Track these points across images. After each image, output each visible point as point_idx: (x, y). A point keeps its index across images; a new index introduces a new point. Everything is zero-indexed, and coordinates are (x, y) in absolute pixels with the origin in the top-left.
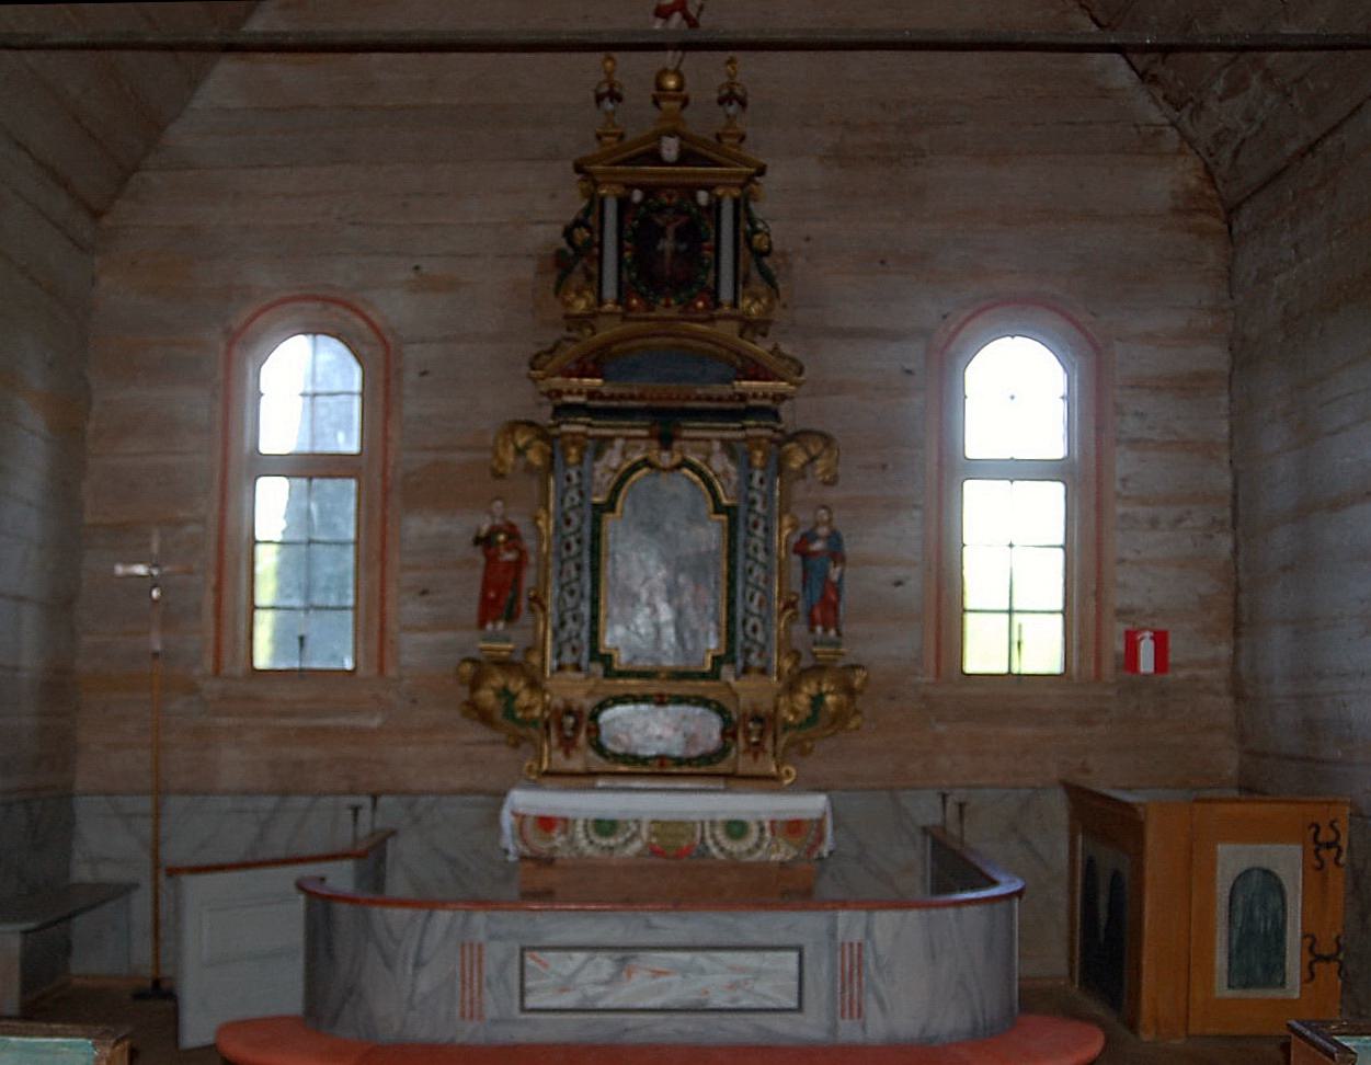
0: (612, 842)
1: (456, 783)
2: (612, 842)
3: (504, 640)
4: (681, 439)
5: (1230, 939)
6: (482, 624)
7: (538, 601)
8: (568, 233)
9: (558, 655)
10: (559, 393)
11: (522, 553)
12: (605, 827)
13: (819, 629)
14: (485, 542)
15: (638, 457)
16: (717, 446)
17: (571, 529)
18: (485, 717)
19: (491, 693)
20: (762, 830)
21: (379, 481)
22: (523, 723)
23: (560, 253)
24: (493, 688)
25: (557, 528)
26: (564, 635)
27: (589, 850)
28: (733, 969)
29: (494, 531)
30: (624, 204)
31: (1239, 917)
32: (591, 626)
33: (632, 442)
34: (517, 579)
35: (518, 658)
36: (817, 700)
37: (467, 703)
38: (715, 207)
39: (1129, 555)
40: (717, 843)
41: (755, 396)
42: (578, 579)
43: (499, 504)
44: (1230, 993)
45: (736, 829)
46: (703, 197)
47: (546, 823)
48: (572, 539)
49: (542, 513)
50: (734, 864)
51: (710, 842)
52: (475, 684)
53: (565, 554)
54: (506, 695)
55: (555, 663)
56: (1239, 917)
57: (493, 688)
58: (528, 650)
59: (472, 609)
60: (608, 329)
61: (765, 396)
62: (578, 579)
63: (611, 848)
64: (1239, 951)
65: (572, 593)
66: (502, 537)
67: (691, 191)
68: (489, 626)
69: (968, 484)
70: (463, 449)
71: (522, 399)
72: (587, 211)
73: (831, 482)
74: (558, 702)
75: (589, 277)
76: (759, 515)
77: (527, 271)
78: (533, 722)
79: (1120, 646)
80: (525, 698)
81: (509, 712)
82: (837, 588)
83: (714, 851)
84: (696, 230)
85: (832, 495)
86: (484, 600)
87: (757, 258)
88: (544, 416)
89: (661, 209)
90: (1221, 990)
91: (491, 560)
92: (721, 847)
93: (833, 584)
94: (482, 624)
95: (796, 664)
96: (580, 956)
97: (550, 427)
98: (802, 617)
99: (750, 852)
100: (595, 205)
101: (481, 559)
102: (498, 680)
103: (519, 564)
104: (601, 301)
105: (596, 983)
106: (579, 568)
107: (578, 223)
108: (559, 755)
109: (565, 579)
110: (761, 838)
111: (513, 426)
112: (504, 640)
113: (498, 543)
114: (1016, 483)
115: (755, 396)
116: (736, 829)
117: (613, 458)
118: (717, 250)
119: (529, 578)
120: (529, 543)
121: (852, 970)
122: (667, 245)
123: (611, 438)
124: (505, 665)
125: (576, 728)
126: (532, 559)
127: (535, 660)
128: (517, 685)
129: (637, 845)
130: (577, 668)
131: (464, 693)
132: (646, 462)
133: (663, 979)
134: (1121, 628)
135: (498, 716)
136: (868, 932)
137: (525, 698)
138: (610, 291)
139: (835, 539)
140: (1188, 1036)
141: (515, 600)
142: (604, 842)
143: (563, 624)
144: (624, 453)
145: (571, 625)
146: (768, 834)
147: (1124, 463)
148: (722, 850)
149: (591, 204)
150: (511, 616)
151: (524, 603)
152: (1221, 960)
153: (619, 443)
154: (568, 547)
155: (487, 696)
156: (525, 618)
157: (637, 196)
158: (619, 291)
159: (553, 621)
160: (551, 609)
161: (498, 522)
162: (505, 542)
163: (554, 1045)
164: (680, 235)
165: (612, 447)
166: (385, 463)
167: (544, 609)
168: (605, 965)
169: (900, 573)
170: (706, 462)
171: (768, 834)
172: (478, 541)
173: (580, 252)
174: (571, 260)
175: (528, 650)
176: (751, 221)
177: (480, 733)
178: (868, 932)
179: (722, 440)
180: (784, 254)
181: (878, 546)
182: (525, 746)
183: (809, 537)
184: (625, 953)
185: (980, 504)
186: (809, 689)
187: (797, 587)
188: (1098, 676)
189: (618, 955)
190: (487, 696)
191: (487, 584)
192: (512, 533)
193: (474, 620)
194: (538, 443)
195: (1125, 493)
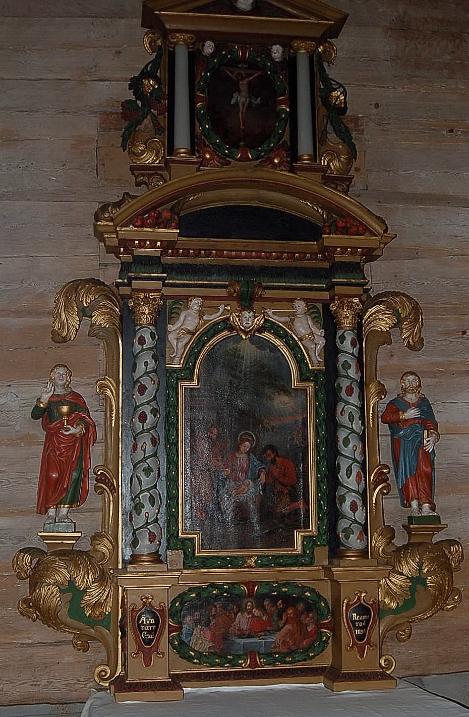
3: (65, 527)
4: (261, 299)
6: (43, 509)
7: (107, 482)
8: (135, 84)
9: (135, 543)
11: (90, 427)
13: (414, 504)
14: (44, 414)
15: (215, 317)
16: (300, 306)
17: (144, 399)
18: (49, 617)
19: (55, 590)
21: (432, 673)
22: (91, 622)
23: (126, 104)
24: (56, 584)
25: (128, 397)
26: (139, 521)
29: (57, 401)
30: (194, 57)
32: (168, 506)
34: (83, 456)
35: (85, 546)
37: (26, 601)
38: (290, 64)
42: (155, 455)
43: (61, 371)
46: (277, 52)
49: (109, 382)
52: (35, 579)
53: (139, 426)
54: (72, 590)
55: (128, 553)
57: (56, 584)
58: (97, 537)
59: (32, 491)
60: (181, 178)
62: (155, 455)
65: (148, 471)
66: (65, 409)
67: (264, 43)
68: (52, 512)
70: (19, 313)
71: (90, 259)
72: (156, 63)
74: (134, 600)
75: (158, 129)
77: (90, 127)
78: (105, 621)
80: (94, 594)
81: (76, 610)
82: (429, 458)
84: (273, 85)
85: (415, 361)
86: (45, 479)
87: (334, 118)
88: (111, 276)
89: (234, 63)
91: (52, 435)
93: (426, 453)
94: (43, 509)
95: (389, 543)
97: (118, 285)
98: (395, 491)
100: (165, 58)
101: (42, 435)
102: (62, 574)
103: (86, 440)
104: (171, 150)
106: (154, 442)
107: (145, 74)
108: (136, 663)
109: (140, 455)
111: (75, 287)
112: (65, 527)
113: (62, 415)
118: (293, 102)
119: (96, 454)
120: (97, 417)
122: (240, 99)
123: (187, 298)
124: (70, 555)
125: (156, 629)
126: (100, 434)
127: (104, 547)
128: (84, 579)
130: (156, 558)
131: (24, 588)
132: (226, 324)
135: (63, 614)
137: (94, 594)
138: (182, 141)
139: (424, 404)
141: (80, 482)
143: (138, 507)
144: (201, 315)
145: (147, 508)
149: (159, 56)
150: (76, 499)
151: (92, 483)
153: (195, 304)
154: (143, 418)
155: (50, 592)
156: (93, 500)
157: (209, 48)
158: (193, 143)
159: (125, 503)
160: (124, 490)
161: (60, 391)
162: (69, 414)
163: (190, 105)
164: (253, 90)
165: (187, 308)
167: (114, 490)
170: (290, 324)
172: (38, 413)
173: (148, 101)
174: (144, 109)
175: (97, 537)
176: (326, 79)
177: (42, 633)
180: (356, 120)
182: (94, 644)
183: (396, 406)
186: (408, 567)
187: (386, 457)
190: (50, 592)
191: (47, 464)
192: (77, 403)
193: (33, 505)
194: (105, 303)
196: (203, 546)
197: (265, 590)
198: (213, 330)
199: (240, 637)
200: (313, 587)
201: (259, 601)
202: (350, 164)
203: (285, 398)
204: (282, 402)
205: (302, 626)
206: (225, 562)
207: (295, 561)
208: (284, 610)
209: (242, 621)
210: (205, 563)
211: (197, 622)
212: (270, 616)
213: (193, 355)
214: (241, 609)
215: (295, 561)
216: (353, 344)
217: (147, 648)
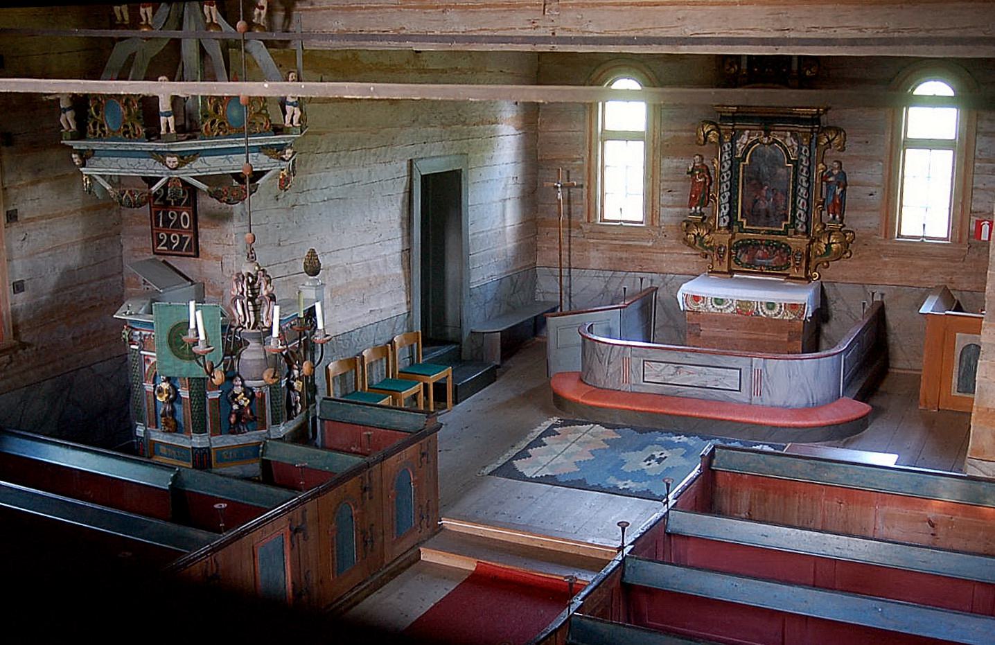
0: (722, 307)
1: (682, 271)
2: (722, 307)
5: (959, 372)
10: (721, 112)
12: (719, 301)
16: (789, 134)
18: (691, 246)
20: (781, 307)
27: (713, 310)
28: (716, 374)
31: (964, 364)
33: (752, 132)
36: (828, 246)
39: (981, 186)
40: (762, 311)
41: (803, 114)
44: (958, 394)
45: (771, 306)
47: (696, 298)
48: (725, 175)
50: (769, 319)
51: (760, 310)
56: (964, 364)
61: (807, 114)
63: (721, 310)
64: (963, 377)
69: (953, 138)
73: (843, 150)
76: (804, 166)
79: (973, 227)
83: (761, 314)
90: (955, 393)
92: (764, 312)
96: (664, 365)
99: (775, 315)
105: (669, 375)
108: (716, 264)
110: (781, 310)
114: (933, 151)
115: (803, 114)
116: (771, 306)
117: (744, 139)
121: (758, 379)
129: (732, 309)
132: (757, 141)
133: (691, 375)
134: (974, 219)
136: (764, 365)
140: (939, 410)
142: (718, 307)
146: (783, 309)
147: (982, 142)
148: (764, 313)
152: (955, 380)
154: (723, 178)
166: (948, 29)
168: (672, 368)
169: (872, 190)
171: (783, 309)
177: (688, 251)
178: (764, 365)
179: (791, 131)
181: (864, 176)
184: (679, 366)
185: (913, 160)
188: (960, 242)
189: (676, 366)
195: (980, 157)
196: (747, 225)
197: (767, 243)
198: (753, 144)
199: (759, 259)
200: (287, 83)
201: (766, 246)
202: (740, 477)
203: (781, 169)
204: (781, 171)
205: (782, 258)
206: (753, 231)
207: (780, 233)
208: (774, 252)
209: (759, 253)
210: (746, 231)
211: (743, 252)
212: (770, 253)
213: (745, 153)
214: (760, 249)
215: (780, 233)
216: (806, 173)
217: (721, 260)
